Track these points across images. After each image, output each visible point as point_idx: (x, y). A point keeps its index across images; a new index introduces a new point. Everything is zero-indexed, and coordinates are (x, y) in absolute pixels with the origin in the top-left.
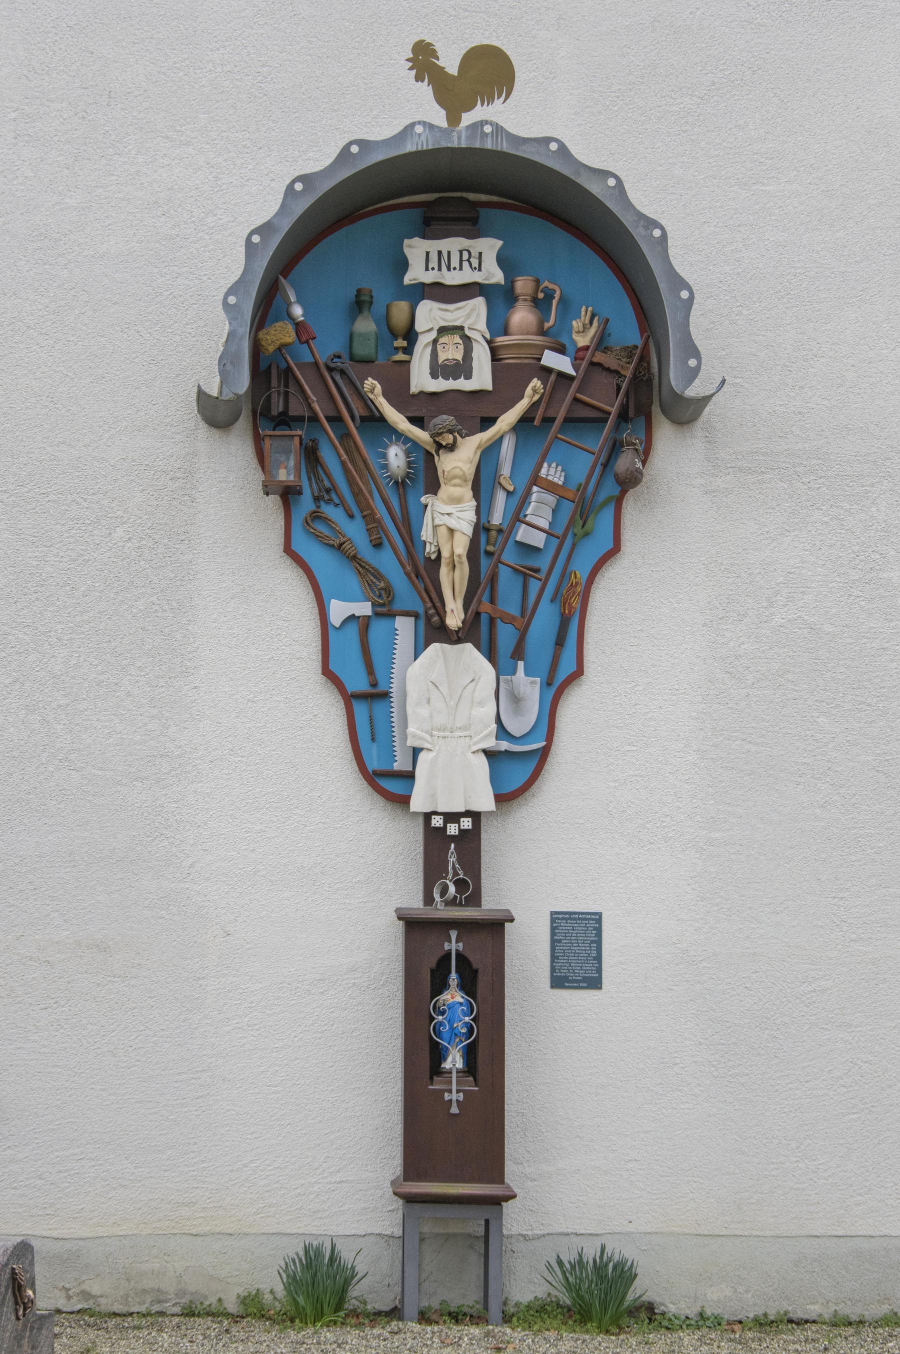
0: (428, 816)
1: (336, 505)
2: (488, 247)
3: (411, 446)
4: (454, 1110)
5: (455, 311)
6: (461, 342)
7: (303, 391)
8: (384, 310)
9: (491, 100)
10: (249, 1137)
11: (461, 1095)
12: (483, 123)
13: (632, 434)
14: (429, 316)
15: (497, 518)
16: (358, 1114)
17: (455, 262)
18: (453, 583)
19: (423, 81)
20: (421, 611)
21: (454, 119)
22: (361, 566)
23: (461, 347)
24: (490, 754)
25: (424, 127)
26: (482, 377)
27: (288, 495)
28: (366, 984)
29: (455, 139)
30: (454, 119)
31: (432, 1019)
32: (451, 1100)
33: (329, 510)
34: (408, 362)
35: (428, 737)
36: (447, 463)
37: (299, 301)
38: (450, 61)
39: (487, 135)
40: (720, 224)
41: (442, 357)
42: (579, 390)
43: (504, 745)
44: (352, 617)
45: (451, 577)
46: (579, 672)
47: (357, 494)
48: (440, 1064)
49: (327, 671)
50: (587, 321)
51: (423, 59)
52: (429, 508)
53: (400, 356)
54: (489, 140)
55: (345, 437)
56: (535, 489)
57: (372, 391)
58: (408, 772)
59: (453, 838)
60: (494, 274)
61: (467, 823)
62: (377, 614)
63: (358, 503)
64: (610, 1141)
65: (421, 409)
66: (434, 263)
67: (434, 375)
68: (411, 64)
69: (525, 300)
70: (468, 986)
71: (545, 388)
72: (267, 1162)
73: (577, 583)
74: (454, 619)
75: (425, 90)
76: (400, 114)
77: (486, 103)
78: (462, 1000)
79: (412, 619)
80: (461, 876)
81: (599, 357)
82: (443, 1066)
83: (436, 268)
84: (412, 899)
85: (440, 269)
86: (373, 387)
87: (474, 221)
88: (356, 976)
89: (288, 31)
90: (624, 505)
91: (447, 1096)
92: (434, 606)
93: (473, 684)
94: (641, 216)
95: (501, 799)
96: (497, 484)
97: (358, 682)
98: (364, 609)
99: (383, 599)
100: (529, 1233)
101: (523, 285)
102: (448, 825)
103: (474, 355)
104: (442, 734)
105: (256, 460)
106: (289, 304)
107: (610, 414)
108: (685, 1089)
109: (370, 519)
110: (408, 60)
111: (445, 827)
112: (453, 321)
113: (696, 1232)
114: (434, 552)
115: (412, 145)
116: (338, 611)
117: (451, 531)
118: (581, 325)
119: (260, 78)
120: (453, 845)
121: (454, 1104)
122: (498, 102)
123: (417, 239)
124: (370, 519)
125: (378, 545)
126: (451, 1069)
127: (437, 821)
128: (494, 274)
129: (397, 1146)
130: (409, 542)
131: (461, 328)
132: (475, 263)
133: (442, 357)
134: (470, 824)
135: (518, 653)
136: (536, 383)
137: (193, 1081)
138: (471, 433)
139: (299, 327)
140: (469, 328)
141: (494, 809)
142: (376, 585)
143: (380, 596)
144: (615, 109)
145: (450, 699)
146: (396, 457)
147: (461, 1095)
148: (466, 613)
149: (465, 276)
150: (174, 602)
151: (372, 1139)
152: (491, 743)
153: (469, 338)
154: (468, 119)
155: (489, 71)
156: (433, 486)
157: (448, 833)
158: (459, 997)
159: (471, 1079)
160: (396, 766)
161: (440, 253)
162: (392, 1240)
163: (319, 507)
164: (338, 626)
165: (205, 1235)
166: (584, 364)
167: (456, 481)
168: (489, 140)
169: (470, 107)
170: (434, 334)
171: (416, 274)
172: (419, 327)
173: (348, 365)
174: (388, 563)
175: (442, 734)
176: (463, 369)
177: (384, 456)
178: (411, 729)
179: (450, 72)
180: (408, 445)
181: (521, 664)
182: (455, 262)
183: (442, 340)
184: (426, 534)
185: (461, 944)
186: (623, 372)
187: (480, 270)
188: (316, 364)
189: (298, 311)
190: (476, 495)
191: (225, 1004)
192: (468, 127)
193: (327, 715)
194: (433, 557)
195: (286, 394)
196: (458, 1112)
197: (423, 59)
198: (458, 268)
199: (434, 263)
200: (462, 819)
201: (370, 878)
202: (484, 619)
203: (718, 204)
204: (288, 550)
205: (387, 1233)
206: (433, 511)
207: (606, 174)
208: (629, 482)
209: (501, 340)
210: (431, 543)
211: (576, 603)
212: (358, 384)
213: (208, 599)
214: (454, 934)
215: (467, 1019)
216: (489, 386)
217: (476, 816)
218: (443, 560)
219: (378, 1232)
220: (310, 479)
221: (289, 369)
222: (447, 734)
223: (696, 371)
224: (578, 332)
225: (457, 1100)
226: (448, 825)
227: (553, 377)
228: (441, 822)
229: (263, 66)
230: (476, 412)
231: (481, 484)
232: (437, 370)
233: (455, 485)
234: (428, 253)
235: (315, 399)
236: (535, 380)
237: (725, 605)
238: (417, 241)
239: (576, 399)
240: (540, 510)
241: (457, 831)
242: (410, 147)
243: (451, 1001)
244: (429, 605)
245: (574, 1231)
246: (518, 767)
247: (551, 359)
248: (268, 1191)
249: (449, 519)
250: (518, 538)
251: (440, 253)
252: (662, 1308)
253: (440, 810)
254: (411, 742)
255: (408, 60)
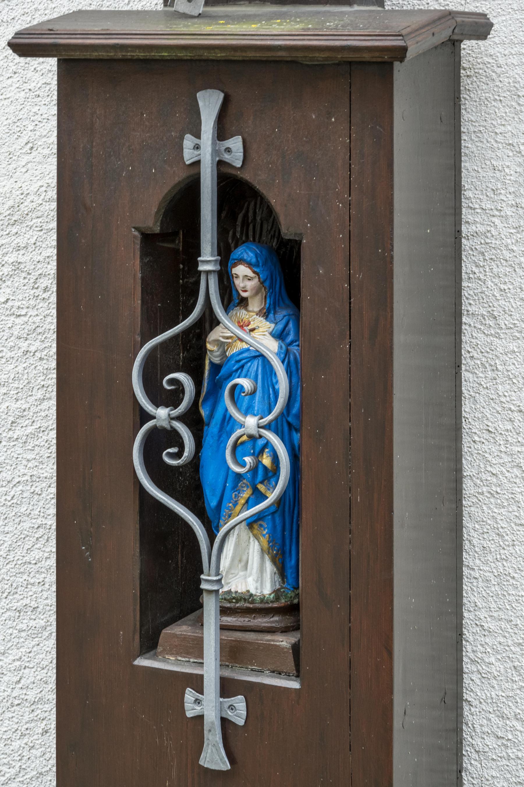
11: (240, 703)
32: (200, 718)
88: (21, 241)
121: (213, 739)
129: (54, 508)
147: (240, 703)
185: (236, 143)
196: (225, 765)
225: (225, 722)
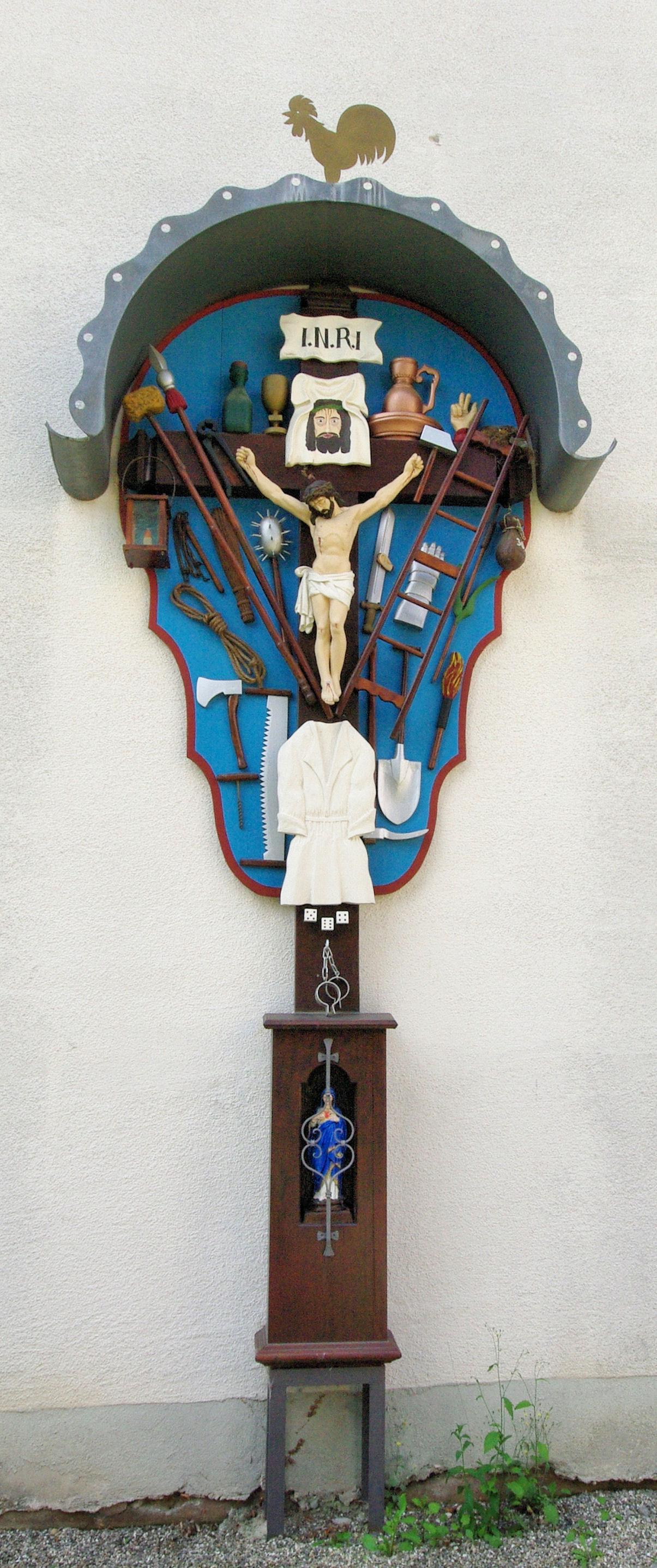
0: (300, 910)
1: (206, 580)
2: (366, 328)
3: (285, 518)
4: (329, 1252)
5: (334, 381)
6: (338, 416)
7: (172, 460)
8: (258, 386)
9: (371, 158)
10: (91, 1286)
12: (362, 181)
13: (512, 513)
14: (305, 389)
15: (376, 598)
16: (218, 1254)
17: (333, 340)
18: (330, 656)
19: (300, 135)
20: (296, 692)
21: (332, 174)
22: (231, 642)
23: (339, 422)
24: (369, 842)
25: (302, 181)
26: (360, 452)
27: (153, 564)
28: (229, 1102)
29: (334, 192)
30: (332, 174)
31: (304, 1143)
33: (195, 584)
34: (285, 435)
35: (301, 823)
36: (322, 531)
37: (172, 369)
38: (329, 118)
39: (367, 191)
40: (591, 329)
41: (319, 430)
42: (460, 468)
43: (383, 833)
44: (221, 695)
45: (327, 651)
46: (461, 757)
47: (229, 569)
48: (312, 1194)
49: (192, 754)
50: (466, 407)
51: (301, 115)
52: (304, 580)
53: (276, 429)
54: (369, 197)
55: (219, 510)
56: (415, 565)
57: (245, 460)
58: (279, 862)
59: (328, 933)
60: (372, 353)
61: (343, 917)
62: (246, 692)
63: (229, 577)
64: (509, 1292)
65: (296, 480)
66: (311, 338)
67: (310, 447)
68: (287, 118)
69: (404, 382)
70: (345, 1104)
71: (424, 464)
72: (111, 1317)
73: (458, 664)
74: (331, 693)
75: (303, 145)
76: (279, 165)
77: (366, 162)
78: (337, 1119)
79: (286, 699)
80: (337, 977)
81: (480, 437)
82: (315, 1197)
83: (313, 343)
84: (282, 1000)
85: (317, 345)
86: (246, 457)
87: (354, 306)
89: (168, 129)
90: (504, 589)
91: (320, 1236)
92: (309, 683)
93: (351, 763)
94: (526, 279)
95: (380, 890)
96: (375, 562)
97: (226, 766)
98: (234, 687)
99: (254, 677)
100: (413, 1386)
101: (403, 367)
102: (323, 919)
103: (352, 429)
104: (316, 819)
105: (120, 526)
106: (158, 372)
107: (489, 493)
108: (581, 1208)
109: (243, 594)
110: (284, 114)
111: (319, 921)
112: (331, 395)
113: (597, 1375)
114: (309, 626)
115: (288, 195)
116: (206, 689)
117: (328, 600)
118: (459, 408)
119: (137, 170)
120: (328, 942)
121: (329, 1246)
122: (378, 162)
123: (294, 315)
124: (243, 594)
125: (250, 622)
126: (325, 1201)
127: (311, 915)
128: (372, 353)
130: (282, 614)
131: (340, 403)
132: (353, 341)
133: (319, 430)
134: (347, 917)
135: (397, 737)
136: (416, 458)
137: (26, 1222)
138: (349, 504)
139: (168, 394)
140: (348, 403)
141: (374, 901)
142: (247, 662)
143: (252, 675)
144: (489, 219)
145: (325, 783)
146: (270, 533)
148: (343, 690)
149: (346, 354)
150: (26, 680)
151: (234, 1282)
152: (369, 828)
153: (346, 412)
154: (347, 175)
155: (369, 130)
156: (308, 557)
157: (323, 928)
158: (334, 1117)
159: (348, 1212)
160: (267, 856)
161: (317, 330)
162: (256, 1404)
163: (187, 581)
164: (205, 705)
165: (34, 1412)
166: (465, 443)
167: (334, 549)
168: (369, 197)
169: (350, 164)
170: (311, 407)
171: (291, 349)
172: (295, 400)
173: (220, 435)
174: (262, 642)
175: (316, 819)
176: (340, 442)
177: (258, 530)
178: (283, 813)
179: (330, 129)
180: (284, 519)
181: (400, 747)
182: (333, 340)
183: (318, 414)
184: (301, 606)
185: (336, 1055)
186: (503, 451)
187: (358, 348)
188: (187, 434)
189: (168, 381)
190: (354, 568)
191: (68, 1128)
192: (347, 183)
193: (190, 797)
194: (308, 631)
195: (154, 464)
197: (301, 115)
198: (335, 345)
199: (311, 338)
200: (338, 913)
201: (243, 973)
202: (362, 696)
203: (589, 310)
204: (154, 626)
205: (250, 1396)
206: (308, 581)
207: (490, 236)
208: (509, 563)
209: (379, 417)
210: (306, 616)
211: (457, 684)
212: (230, 454)
213: (64, 677)
214: (328, 1043)
215: (343, 1142)
216: (366, 460)
217: (353, 909)
218: (318, 631)
219: (239, 1396)
220: (178, 555)
221: (157, 439)
222: (322, 818)
223: (586, 432)
224: (458, 416)
226: (323, 919)
227: (433, 454)
228: (315, 915)
229: (143, 158)
230: (353, 485)
231: (360, 557)
232: (313, 442)
233: (332, 553)
234: (305, 330)
235: (184, 467)
236: (415, 455)
237: (607, 691)
238: (294, 317)
239: (456, 478)
240: (421, 582)
241: (332, 926)
242: (286, 198)
243: (326, 1120)
244: (303, 680)
245: (463, 1381)
246: (397, 858)
247: (431, 435)
248: (110, 1353)
249: (325, 591)
250: (397, 618)
251: (317, 330)
252: (562, 1468)
253: (313, 903)
254: (283, 828)
255: (284, 114)
